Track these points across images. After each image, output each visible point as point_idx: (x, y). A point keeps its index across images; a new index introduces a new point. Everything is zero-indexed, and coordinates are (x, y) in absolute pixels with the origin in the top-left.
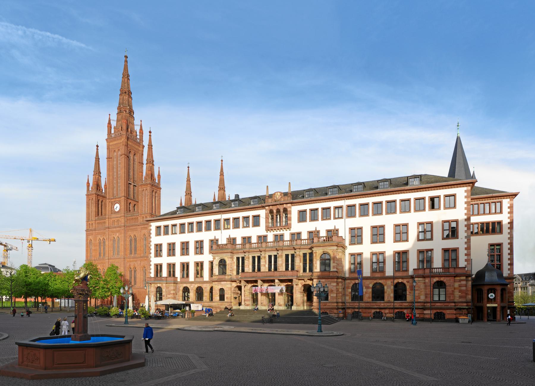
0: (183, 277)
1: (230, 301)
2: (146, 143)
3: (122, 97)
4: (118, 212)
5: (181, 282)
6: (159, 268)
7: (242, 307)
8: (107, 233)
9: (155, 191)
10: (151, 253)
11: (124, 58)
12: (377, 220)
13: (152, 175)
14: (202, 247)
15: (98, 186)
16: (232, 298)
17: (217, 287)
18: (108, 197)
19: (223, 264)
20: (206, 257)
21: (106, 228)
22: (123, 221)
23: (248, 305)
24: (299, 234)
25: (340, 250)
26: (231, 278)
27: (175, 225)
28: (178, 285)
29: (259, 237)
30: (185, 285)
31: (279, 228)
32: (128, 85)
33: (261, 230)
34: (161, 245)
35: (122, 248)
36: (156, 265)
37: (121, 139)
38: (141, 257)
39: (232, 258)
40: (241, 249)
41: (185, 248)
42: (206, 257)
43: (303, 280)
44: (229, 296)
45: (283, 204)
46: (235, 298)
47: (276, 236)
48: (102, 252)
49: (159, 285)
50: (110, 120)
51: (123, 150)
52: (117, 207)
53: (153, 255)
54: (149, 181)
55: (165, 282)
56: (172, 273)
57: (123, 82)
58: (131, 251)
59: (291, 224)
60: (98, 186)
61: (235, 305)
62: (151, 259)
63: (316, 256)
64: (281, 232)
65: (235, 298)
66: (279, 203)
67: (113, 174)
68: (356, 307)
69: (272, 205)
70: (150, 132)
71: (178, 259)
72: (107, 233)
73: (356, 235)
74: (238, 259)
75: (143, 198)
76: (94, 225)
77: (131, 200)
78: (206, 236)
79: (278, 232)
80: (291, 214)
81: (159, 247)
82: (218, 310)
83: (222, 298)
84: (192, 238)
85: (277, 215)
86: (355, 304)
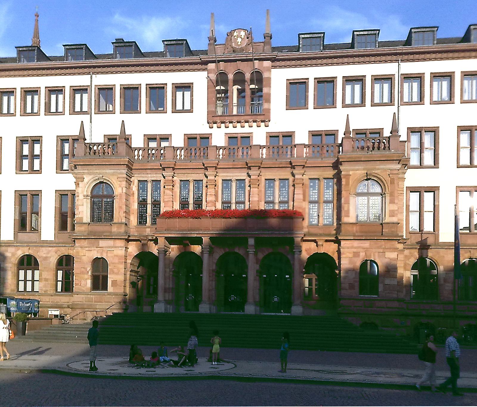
12: (28, 127)
24: (289, 136)
27: (34, 92)
29: (190, 138)
33: (197, 123)
39: (129, 182)
43: (315, 241)
47: (232, 138)
63: (347, 184)
64: (246, 129)
69: (225, 61)
79: (239, 130)
80: (269, 86)
83: (99, 282)
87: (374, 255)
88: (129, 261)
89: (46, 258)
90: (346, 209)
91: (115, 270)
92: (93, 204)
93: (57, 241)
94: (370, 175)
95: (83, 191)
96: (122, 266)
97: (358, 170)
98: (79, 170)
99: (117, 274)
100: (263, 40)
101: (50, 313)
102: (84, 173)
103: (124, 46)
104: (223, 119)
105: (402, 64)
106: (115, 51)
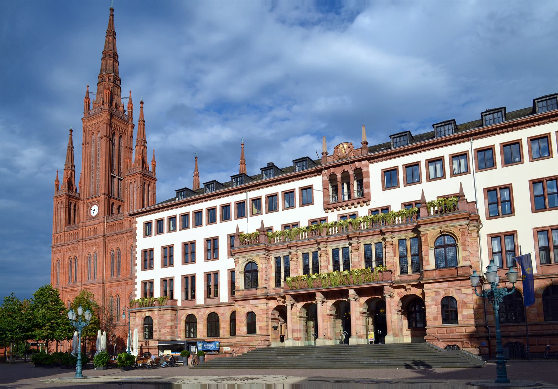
0: (187, 298)
1: (265, 333)
2: (136, 121)
3: (104, 62)
4: (96, 216)
5: (183, 308)
6: (148, 285)
7: (288, 343)
8: (80, 248)
9: (147, 182)
10: (136, 265)
11: (109, 12)
13: (144, 162)
14: (216, 249)
15: (70, 184)
16: (270, 327)
17: (242, 310)
18: (82, 198)
19: (252, 274)
20: (224, 264)
21: (79, 241)
22: (102, 229)
23: (297, 339)
24: (386, 209)
25: (474, 223)
26: (267, 293)
28: (179, 313)
30: (189, 312)
31: (349, 203)
32: (114, 45)
33: (316, 210)
34: (151, 250)
35: (100, 268)
36: (144, 283)
37: (102, 116)
38: (127, 279)
39: (268, 260)
40: (283, 242)
41: (189, 252)
42: (224, 264)
43: (403, 287)
44: (264, 324)
45: (353, 162)
46: (275, 328)
48: (73, 275)
49: (147, 314)
50: (88, 94)
51: (104, 130)
52: (95, 210)
53: (139, 267)
54: (139, 170)
55: (157, 308)
56: (168, 293)
57: (107, 42)
58: (112, 270)
59: (369, 194)
60: (70, 184)
61: (275, 339)
62: (136, 274)
63: (426, 241)
64: (353, 210)
65: (275, 328)
66: (345, 161)
67: (90, 164)
68: (512, 334)
70: (142, 103)
71: (178, 271)
72: (80, 248)
73: (500, 201)
74: (277, 259)
75: (131, 194)
76: (63, 238)
77: (115, 199)
78: (222, 230)
81: (148, 254)
82: (246, 351)
83: (251, 328)
84: (198, 235)
85: (343, 184)
86: (509, 329)
87: (452, 292)
88: (270, 312)
89: (223, 314)
90: (426, 259)
91: (261, 319)
92: (246, 276)
93: (230, 302)
94: (444, 231)
95: (240, 270)
96: (265, 316)
97: (433, 229)
98: (237, 256)
99: (262, 321)
100: (361, 146)
101: (224, 350)
102: (239, 258)
103: (213, 184)
104: (334, 205)
105: (249, 193)
106: (262, 173)
